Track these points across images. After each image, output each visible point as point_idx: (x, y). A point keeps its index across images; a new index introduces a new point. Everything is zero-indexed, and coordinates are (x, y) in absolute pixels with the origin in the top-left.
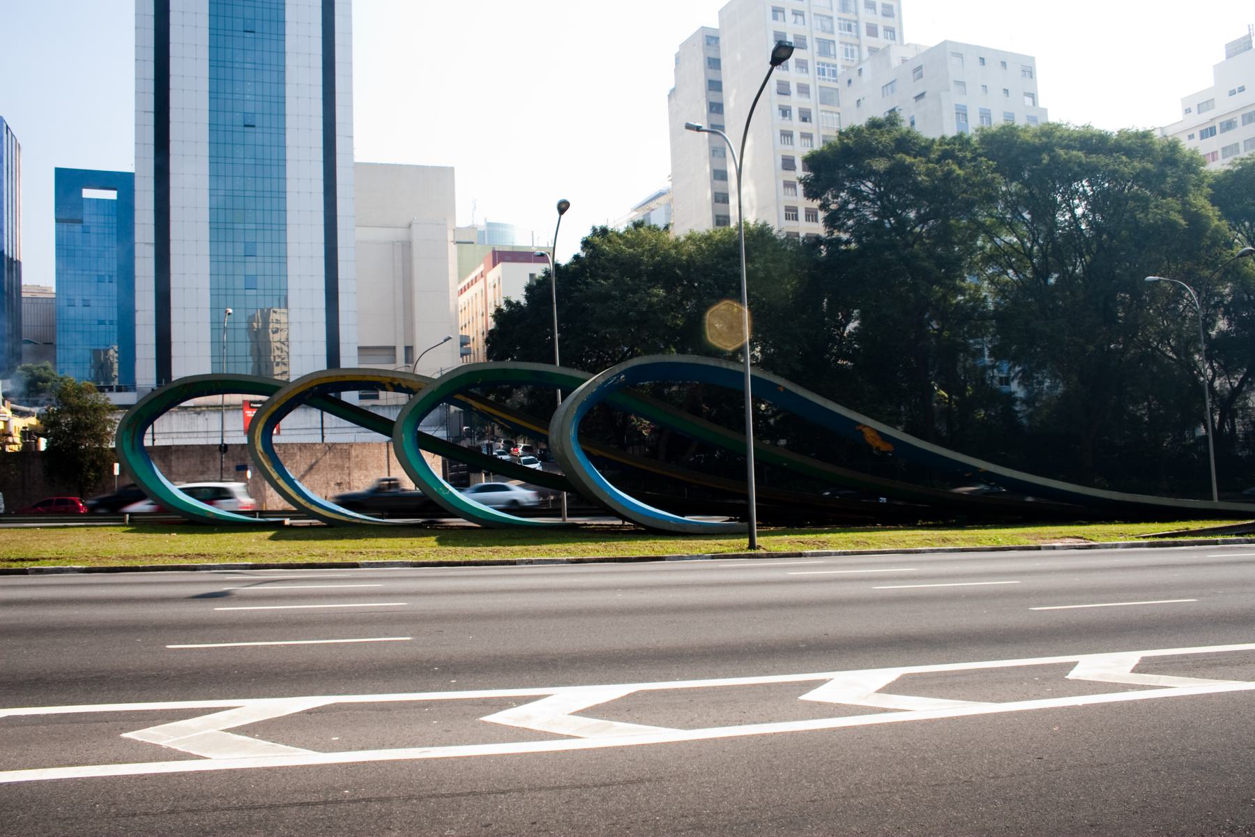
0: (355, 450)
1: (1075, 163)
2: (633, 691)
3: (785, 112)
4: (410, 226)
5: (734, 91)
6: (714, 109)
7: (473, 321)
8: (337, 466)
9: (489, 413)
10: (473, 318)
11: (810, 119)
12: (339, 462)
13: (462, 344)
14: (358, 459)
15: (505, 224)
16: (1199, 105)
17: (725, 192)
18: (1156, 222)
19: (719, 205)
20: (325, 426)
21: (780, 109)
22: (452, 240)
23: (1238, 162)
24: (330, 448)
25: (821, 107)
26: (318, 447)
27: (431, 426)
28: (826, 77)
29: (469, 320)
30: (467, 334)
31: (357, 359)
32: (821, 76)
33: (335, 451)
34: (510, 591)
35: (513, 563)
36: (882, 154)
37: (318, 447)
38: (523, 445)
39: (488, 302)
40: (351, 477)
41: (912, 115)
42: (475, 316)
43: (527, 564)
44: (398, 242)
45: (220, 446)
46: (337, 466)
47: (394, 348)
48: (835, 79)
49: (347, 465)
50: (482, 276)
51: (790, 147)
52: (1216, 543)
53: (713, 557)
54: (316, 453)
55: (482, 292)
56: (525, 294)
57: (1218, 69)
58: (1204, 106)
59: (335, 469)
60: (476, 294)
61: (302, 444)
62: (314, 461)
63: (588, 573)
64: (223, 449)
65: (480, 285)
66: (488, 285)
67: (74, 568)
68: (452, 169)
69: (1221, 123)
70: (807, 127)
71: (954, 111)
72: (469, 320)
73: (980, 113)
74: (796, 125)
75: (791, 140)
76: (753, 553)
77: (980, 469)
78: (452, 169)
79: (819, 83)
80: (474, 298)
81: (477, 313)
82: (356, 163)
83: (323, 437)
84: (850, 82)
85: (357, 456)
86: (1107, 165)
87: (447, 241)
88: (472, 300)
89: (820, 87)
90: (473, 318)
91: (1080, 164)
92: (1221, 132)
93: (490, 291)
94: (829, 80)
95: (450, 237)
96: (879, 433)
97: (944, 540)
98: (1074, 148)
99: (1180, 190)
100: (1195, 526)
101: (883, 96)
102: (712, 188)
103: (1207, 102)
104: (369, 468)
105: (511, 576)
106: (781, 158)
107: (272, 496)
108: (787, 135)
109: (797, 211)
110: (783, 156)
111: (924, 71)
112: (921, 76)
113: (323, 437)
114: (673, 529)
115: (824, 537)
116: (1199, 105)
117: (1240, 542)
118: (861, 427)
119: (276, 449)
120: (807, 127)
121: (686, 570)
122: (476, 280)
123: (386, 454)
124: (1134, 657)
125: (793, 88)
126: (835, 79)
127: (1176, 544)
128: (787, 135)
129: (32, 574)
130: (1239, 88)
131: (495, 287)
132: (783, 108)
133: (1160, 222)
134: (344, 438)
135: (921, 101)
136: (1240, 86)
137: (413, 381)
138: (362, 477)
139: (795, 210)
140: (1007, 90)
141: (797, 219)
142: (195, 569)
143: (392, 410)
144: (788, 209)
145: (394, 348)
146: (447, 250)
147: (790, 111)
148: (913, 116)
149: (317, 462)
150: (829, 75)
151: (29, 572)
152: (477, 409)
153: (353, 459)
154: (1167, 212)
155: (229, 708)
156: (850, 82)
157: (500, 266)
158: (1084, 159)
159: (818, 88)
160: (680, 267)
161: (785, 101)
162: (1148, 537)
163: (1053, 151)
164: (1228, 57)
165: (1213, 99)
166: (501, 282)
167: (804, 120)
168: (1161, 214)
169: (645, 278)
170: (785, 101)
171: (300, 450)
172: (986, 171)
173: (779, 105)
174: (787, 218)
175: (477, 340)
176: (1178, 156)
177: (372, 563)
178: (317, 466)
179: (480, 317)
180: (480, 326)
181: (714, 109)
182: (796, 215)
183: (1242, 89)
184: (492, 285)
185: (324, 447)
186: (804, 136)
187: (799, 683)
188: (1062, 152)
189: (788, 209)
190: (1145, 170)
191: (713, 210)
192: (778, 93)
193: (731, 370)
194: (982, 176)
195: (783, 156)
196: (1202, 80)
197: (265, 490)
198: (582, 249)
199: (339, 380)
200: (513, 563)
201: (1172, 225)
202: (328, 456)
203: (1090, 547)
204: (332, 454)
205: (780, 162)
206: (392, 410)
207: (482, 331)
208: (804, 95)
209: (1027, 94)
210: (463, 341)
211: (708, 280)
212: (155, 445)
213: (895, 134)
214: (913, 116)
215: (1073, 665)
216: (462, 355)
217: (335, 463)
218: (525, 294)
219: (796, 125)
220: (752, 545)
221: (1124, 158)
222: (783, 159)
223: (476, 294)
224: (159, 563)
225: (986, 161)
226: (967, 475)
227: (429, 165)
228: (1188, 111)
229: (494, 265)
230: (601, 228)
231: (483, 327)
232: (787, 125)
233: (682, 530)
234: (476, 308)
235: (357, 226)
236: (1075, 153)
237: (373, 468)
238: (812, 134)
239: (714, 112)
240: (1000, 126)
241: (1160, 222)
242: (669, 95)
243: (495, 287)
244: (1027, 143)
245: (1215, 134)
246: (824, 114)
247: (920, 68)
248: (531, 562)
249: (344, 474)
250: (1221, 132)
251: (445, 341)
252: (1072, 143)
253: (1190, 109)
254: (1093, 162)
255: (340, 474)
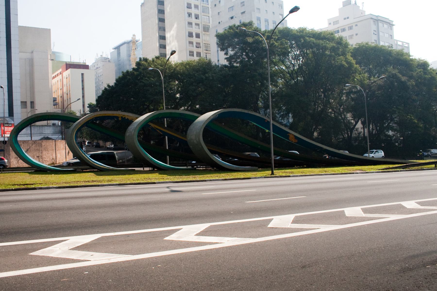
0: (44, 143)
1: (312, 42)
2: (96, 238)
3: (190, 15)
4: (32, 52)
5: (169, 6)
6: (160, 12)
7: (56, 92)
8: (37, 150)
9: (156, 128)
10: (56, 90)
11: (199, 18)
12: (38, 147)
13: (54, 101)
14: (45, 147)
15: (59, 52)
16: (334, 22)
17: (164, 44)
18: (338, 65)
19: (161, 49)
20: (32, 133)
21: (188, 14)
22: (50, 58)
23: (358, 45)
24: (34, 142)
25: (202, 14)
26: (30, 142)
27: (56, 134)
28: (205, 2)
29: (54, 91)
30: (55, 97)
31: (20, 107)
32: (203, 2)
33: (36, 143)
34: (292, 184)
35: (205, 181)
36: (249, 36)
37: (30, 142)
38: (87, 141)
39: (64, 84)
40: (43, 154)
41: (240, 19)
42: (57, 90)
43: (210, 181)
44: (27, 59)
45: (3, 141)
46: (37, 150)
47: (26, 102)
48: (208, 3)
49: (41, 149)
50: (61, 74)
51: (191, 28)
52: (398, 171)
53: (265, 178)
54: (29, 144)
55: (61, 80)
56: (115, 82)
57: (340, 10)
58: (336, 22)
59: (36, 151)
60: (58, 81)
61: (24, 141)
62: (28, 147)
63: (229, 184)
64: (5, 143)
65: (60, 76)
66: (63, 77)
67: (54, 187)
68: (50, 30)
69: (341, 29)
70: (197, 21)
71: (256, 19)
72: (54, 91)
73: (265, 20)
74: (193, 20)
75: (192, 26)
76: (273, 175)
77: (324, 148)
78: (50, 30)
79: (202, 5)
80: (57, 82)
81: (58, 88)
82: (20, 27)
83: (31, 138)
84: (215, 5)
85: (45, 146)
86: (322, 44)
87: (48, 59)
88: (56, 83)
89: (202, 6)
90: (56, 90)
91: (314, 43)
92: (341, 32)
93: (65, 80)
94: (206, 4)
95: (49, 58)
96: (295, 136)
97: (325, 171)
98: (311, 37)
99: (344, 54)
100: (391, 166)
101: (229, 12)
102: (159, 42)
103: (336, 21)
104: (49, 150)
105: (248, 182)
106: (188, 32)
107: (13, 162)
108: (190, 24)
109: (193, 53)
110: (188, 32)
111: (245, 3)
112: (244, 5)
113: (31, 138)
114: (235, 169)
115: (293, 170)
116: (334, 22)
117: (404, 171)
118: (289, 134)
119: (19, 142)
120: (197, 21)
121: (204, 185)
122: (58, 75)
123: (54, 145)
124: (292, 217)
125: (193, 6)
126: (208, 3)
127: (388, 172)
128: (190, 24)
129: (38, 189)
130: (347, 17)
131: (67, 78)
132: (189, 13)
133: (339, 65)
134: (23, 139)
135: (244, 15)
136: (348, 17)
137: (131, 116)
138: (46, 154)
139: (193, 52)
140: (274, 13)
141: (193, 56)
142: (98, 186)
143: (40, 127)
144: (190, 52)
145: (26, 102)
146: (48, 62)
147: (192, 15)
148: (241, 20)
149: (29, 148)
150: (205, 2)
151: (37, 189)
152: (152, 127)
153: (43, 147)
154: (341, 61)
155: (62, 241)
156: (215, 5)
157: (69, 70)
158: (315, 42)
159: (201, 7)
160: (181, 75)
161: (190, 11)
162: (380, 170)
163: (305, 38)
164: (344, 6)
165: (338, 21)
166: (70, 76)
167: (196, 18)
168: (339, 62)
169: (168, 78)
170: (190, 11)
171: (23, 143)
172: (285, 44)
173: (188, 12)
174: (190, 55)
175: (58, 99)
176: (342, 42)
177: (160, 182)
178: (30, 149)
179: (59, 90)
180: (60, 94)
181: (160, 12)
182: (193, 54)
183: (348, 18)
184: (66, 77)
185: (32, 142)
186: (197, 25)
187: (49, 242)
188: (307, 38)
189: (190, 52)
190: (334, 47)
191: (159, 51)
192: (187, 8)
193: (250, 114)
194: (283, 46)
195: (188, 32)
196: (335, 14)
197: (10, 159)
198: (136, 66)
199: (104, 115)
200: (154, 183)
201: (343, 66)
202: (34, 146)
203: (367, 173)
204: (35, 145)
205: (187, 34)
206: (40, 127)
207: (60, 96)
208: (196, 9)
209: (280, 14)
210: (54, 100)
211: (191, 80)
212: (5, 140)
213: (253, 29)
214: (241, 20)
215: (270, 220)
216: (54, 105)
217: (36, 148)
218: (115, 82)
219: (193, 20)
220: (273, 173)
221: (328, 42)
222: (188, 33)
223: (58, 81)
224: (79, 184)
225: (285, 40)
226: (318, 150)
227: (40, 28)
228: (330, 24)
229: (67, 69)
230: (143, 58)
231: (61, 94)
232: (190, 20)
233: (237, 170)
234: (58, 86)
235: (19, 52)
236: (312, 39)
237: (50, 150)
238: (199, 24)
239: (160, 13)
240: (284, 27)
241: (339, 65)
242: (141, 5)
243: (67, 78)
244: (295, 34)
245: (339, 32)
246: (203, 16)
247: (244, 2)
248: (211, 180)
249: (40, 153)
250: (341, 32)
251: (78, 100)
252: (310, 35)
253: (330, 23)
254: (318, 42)
255: (38, 153)
